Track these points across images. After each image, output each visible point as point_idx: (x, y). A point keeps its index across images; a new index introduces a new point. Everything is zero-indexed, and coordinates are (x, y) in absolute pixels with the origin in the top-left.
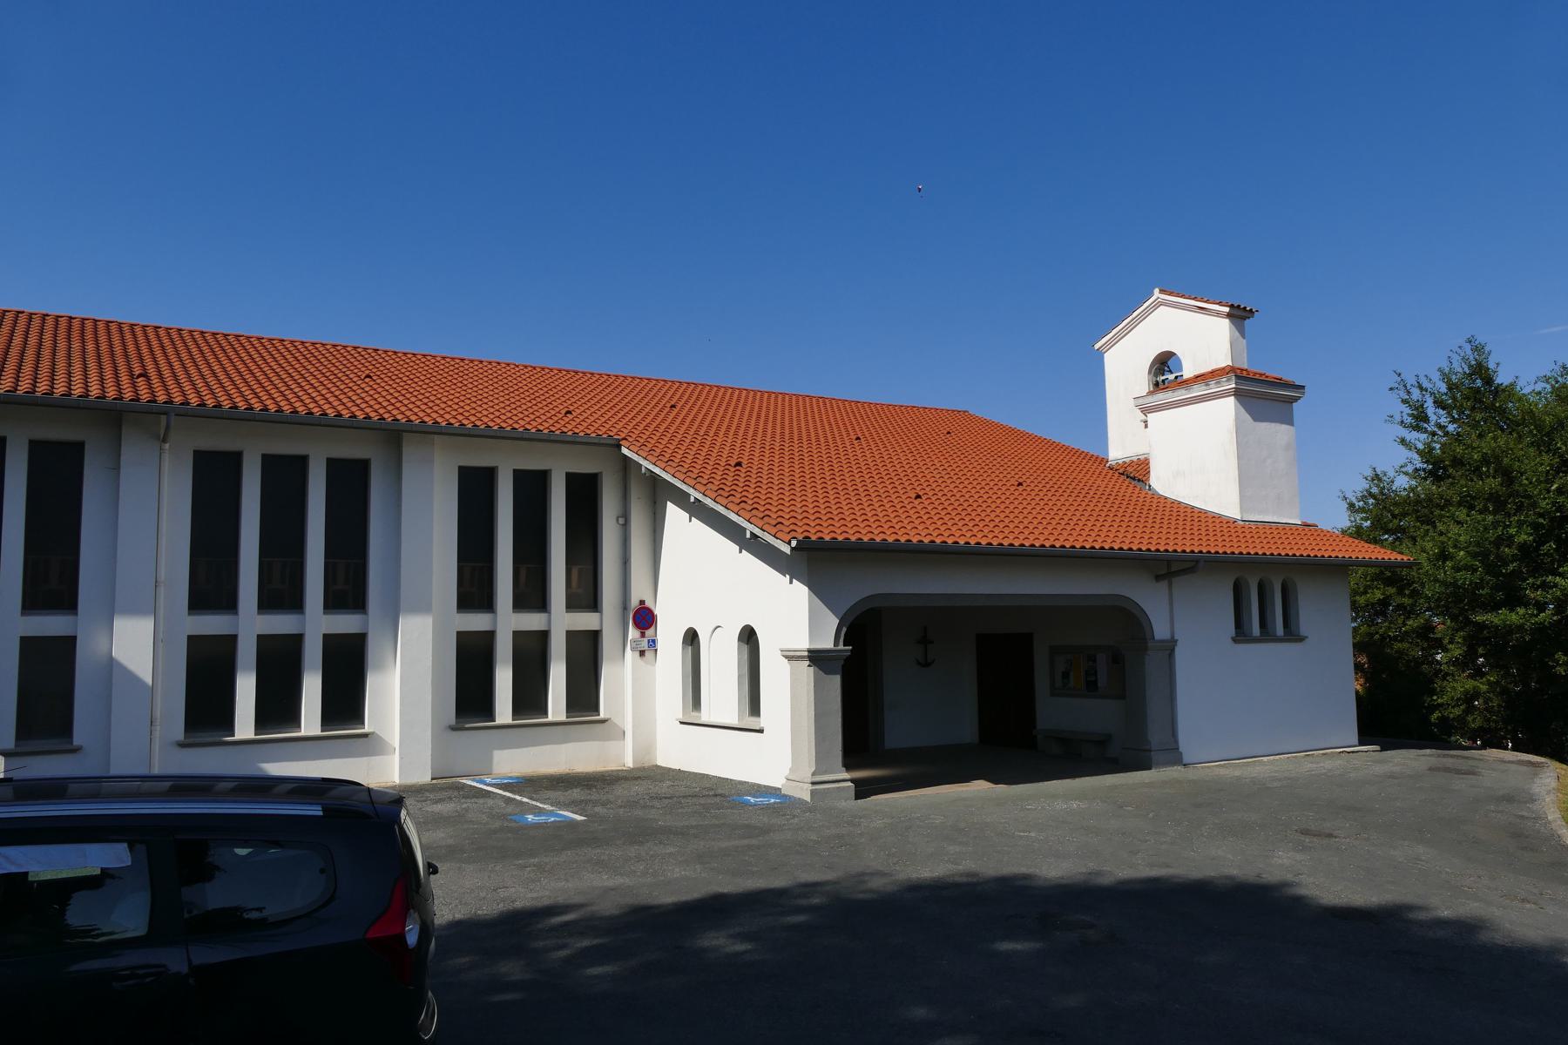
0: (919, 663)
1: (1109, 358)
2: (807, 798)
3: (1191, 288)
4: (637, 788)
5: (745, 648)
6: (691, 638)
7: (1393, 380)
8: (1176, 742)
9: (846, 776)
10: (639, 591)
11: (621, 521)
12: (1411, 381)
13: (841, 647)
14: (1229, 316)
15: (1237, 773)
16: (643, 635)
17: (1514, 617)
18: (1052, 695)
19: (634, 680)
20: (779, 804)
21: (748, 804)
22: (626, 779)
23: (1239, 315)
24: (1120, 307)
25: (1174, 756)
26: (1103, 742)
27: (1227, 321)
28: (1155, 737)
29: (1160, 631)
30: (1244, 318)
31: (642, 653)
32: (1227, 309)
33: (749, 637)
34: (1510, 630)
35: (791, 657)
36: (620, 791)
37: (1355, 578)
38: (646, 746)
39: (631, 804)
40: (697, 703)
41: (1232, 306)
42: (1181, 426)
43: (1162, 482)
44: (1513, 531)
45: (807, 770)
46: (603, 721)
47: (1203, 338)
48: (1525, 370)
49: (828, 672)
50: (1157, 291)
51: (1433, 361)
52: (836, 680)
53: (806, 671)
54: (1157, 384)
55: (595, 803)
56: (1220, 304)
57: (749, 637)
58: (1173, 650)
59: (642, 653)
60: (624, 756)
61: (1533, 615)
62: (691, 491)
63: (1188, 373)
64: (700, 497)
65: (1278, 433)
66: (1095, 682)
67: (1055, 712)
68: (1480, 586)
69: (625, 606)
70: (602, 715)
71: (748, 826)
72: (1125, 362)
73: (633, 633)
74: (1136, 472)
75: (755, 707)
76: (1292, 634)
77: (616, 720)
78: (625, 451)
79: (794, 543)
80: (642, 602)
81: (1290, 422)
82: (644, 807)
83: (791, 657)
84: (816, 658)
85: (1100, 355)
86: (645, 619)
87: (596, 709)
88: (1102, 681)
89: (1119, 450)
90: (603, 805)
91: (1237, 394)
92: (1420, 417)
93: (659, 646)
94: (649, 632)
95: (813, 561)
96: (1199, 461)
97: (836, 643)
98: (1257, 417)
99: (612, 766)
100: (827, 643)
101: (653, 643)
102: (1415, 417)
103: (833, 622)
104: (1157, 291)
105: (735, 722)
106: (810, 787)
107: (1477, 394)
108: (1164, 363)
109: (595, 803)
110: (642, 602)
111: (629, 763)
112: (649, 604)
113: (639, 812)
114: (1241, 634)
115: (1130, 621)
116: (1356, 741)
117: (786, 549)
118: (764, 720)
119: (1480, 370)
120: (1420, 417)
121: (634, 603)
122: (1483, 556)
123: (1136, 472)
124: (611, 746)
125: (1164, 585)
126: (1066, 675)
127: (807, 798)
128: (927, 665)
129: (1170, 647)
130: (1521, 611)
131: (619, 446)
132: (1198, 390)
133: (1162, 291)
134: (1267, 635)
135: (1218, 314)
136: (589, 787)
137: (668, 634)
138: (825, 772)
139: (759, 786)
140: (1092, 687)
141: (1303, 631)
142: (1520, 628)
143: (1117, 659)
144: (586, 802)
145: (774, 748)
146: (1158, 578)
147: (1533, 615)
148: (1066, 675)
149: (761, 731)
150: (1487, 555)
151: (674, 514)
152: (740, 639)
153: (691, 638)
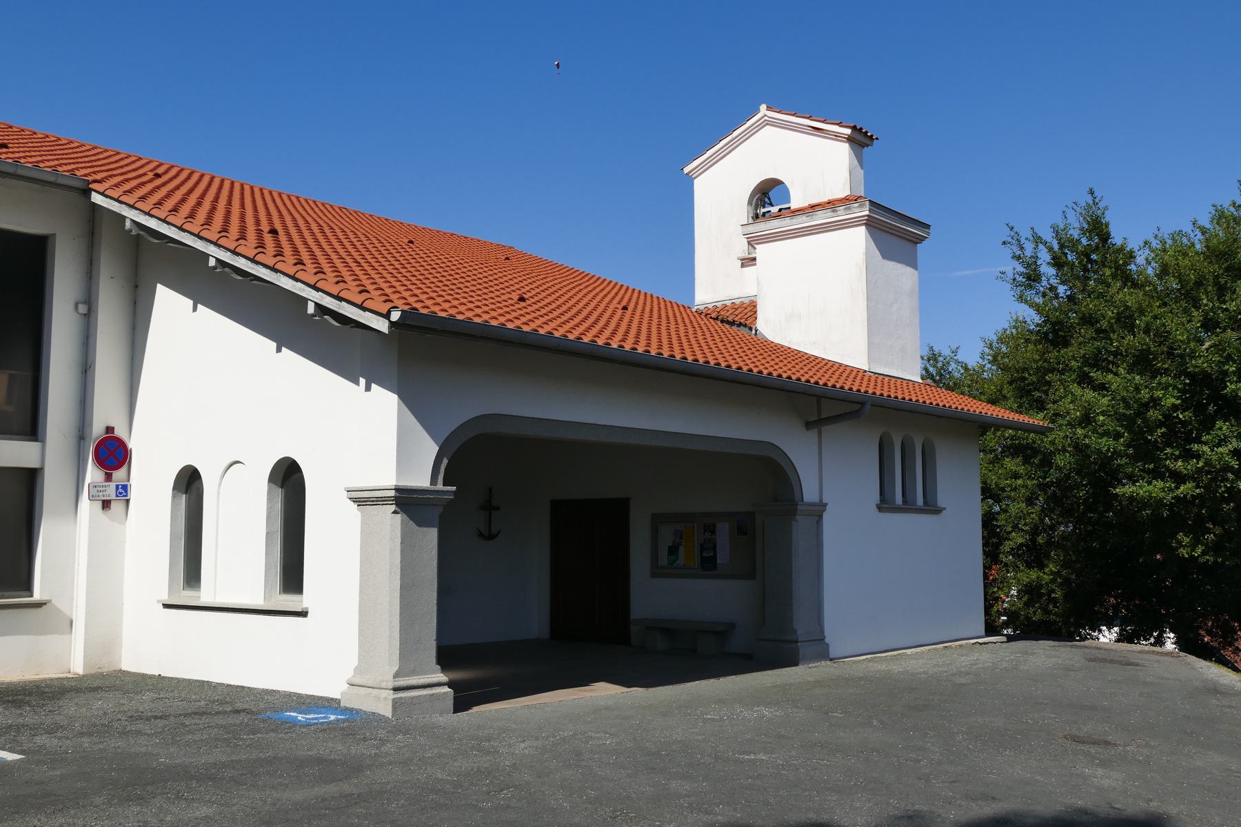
0: (481, 535)
1: (698, 184)
2: (386, 711)
3: (807, 104)
4: (100, 705)
5: (279, 493)
6: (189, 482)
7: (1005, 234)
8: (822, 631)
9: (442, 677)
10: (105, 413)
11: (83, 309)
12: (1025, 233)
13: (440, 487)
14: (850, 139)
15: (883, 667)
16: (109, 478)
17: (1156, 489)
18: (654, 575)
19: (91, 543)
20: (353, 724)
21: (294, 723)
22: (77, 690)
23: (860, 140)
24: (718, 124)
25: (823, 653)
26: (722, 632)
27: (847, 145)
28: (801, 627)
29: (810, 493)
30: (863, 145)
31: (106, 504)
32: (848, 131)
33: (288, 477)
34: (1144, 503)
35: (363, 500)
36: (71, 707)
37: (991, 439)
38: (105, 639)
39: (100, 729)
40: (192, 575)
41: (854, 128)
42: (794, 256)
43: (773, 326)
44: (1159, 393)
45: (386, 668)
46: (39, 605)
47: (816, 163)
48: (1155, 218)
49: (421, 522)
50: (763, 107)
51: (1051, 214)
52: (431, 536)
53: (389, 521)
54: (756, 217)
55: (34, 730)
56: (840, 124)
57: (288, 477)
58: (821, 516)
59: (106, 504)
60: (71, 657)
61: (1171, 490)
62: (211, 250)
63: (795, 204)
64: (226, 257)
65: (903, 276)
66: (713, 559)
67: (653, 596)
68: (1117, 454)
69: (82, 435)
70: (37, 595)
71: (319, 761)
72: (720, 189)
73: (93, 474)
74: (738, 318)
75: (292, 577)
76: (931, 507)
77: (58, 603)
78: (97, 198)
79: (395, 316)
80: (110, 429)
81: (913, 263)
82: (124, 734)
83: (363, 500)
84: (407, 501)
85: (689, 181)
86: (113, 454)
87: (27, 587)
88: (723, 557)
89: (714, 284)
90: (50, 731)
91: (870, 224)
92: (1032, 277)
93: (134, 495)
94: (119, 475)
95: (417, 352)
96: (822, 302)
97: (434, 480)
98: (886, 255)
99: (49, 672)
100: (421, 479)
101: (123, 490)
102: (1029, 278)
103: (430, 449)
104: (763, 107)
105: (258, 602)
106: (391, 695)
107: (1091, 255)
108: (767, 195)
109: (34, 730)
110: (110, 429)
111: (77, 667)
112: (120, 432)
113: (115, 743)
114: (885, 504)
115: (773, 478)
116: (983, 632)
117: (382, 325)
118: (308, 598)
119: (1098, 228)
120: (1032, 277)
121: (97, 430)
122: (1127, 422)
123: (738, 318)
124: (49, 643)
125: (812, 435)
126: (673, 550)
127: (386, 711)
128: (491, 537)
129: (818, 511)
130: (1160, 484)
131: (87, 192)
132: (821, 218)
133: (769, 108)
134: (908, 506)
135: (837, 137)
136: (18, 704)
137: (151, 479)
138: (413, 673)
139: (299, 696)
140: (708, 565)
141: (941, 502)
142: (1160, 503)
143: (745, 528)
144: (19, 728)
145: (338, 640)
146: (809, 425)
147: (1171, 490)
148: (673, 550)
149: (303, 614)
150: (1134, 418)
151: (168, 304)
152: (272, 478)
153: (189, 482)
